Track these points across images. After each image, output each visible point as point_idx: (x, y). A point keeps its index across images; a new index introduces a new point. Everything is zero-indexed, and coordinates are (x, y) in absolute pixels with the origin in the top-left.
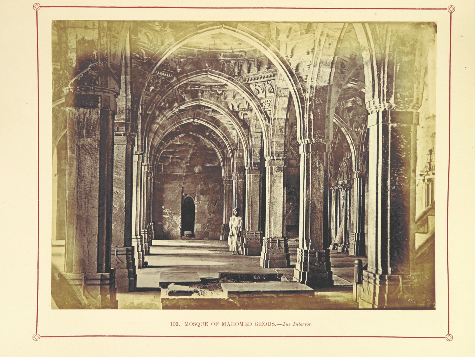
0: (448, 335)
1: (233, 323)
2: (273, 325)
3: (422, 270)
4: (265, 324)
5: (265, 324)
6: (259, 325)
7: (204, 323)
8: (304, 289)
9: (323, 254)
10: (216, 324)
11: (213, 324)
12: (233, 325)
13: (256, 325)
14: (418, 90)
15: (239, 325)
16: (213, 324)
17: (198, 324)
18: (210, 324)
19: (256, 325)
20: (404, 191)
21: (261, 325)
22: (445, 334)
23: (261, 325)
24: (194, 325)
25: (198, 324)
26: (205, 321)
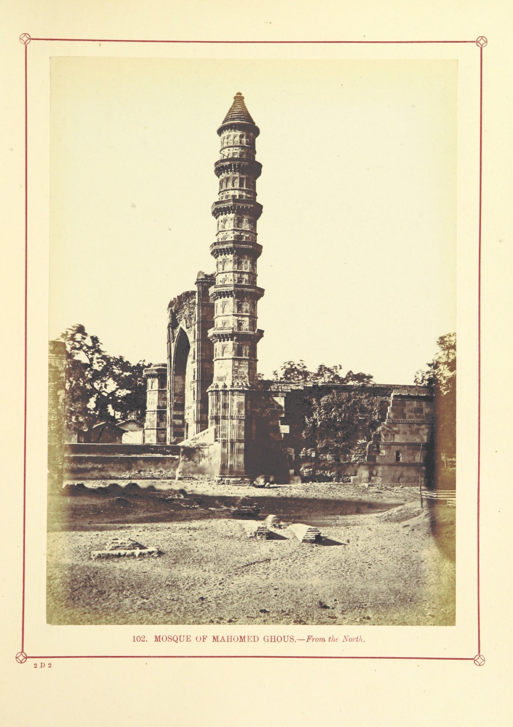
0: (478, 656)
1: (229, 637)
2: (292, 640)
3: (353, 454)
4: (279, 639)
5: (279, 639)
6: (270, 640)
7: (185, 638)
8: (141, 481)
9: (273, 388)
10: (204, 638)
11: (199, 639)
12: (229, 640)
13: (266, 640)
14: (39, 665)
15: (239, 640)
16: (199, 639)
17: (175, 639)
18: (193, 639)
19: (266, 640)
20: (67, 517)
21: (273, 640)
22: (474, 653)
23: (273, 640)
24: (170, 640)
25: (175, 639)
26: (186, 635)
